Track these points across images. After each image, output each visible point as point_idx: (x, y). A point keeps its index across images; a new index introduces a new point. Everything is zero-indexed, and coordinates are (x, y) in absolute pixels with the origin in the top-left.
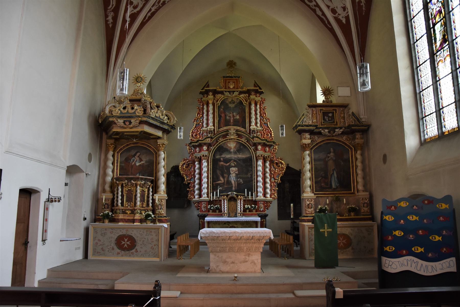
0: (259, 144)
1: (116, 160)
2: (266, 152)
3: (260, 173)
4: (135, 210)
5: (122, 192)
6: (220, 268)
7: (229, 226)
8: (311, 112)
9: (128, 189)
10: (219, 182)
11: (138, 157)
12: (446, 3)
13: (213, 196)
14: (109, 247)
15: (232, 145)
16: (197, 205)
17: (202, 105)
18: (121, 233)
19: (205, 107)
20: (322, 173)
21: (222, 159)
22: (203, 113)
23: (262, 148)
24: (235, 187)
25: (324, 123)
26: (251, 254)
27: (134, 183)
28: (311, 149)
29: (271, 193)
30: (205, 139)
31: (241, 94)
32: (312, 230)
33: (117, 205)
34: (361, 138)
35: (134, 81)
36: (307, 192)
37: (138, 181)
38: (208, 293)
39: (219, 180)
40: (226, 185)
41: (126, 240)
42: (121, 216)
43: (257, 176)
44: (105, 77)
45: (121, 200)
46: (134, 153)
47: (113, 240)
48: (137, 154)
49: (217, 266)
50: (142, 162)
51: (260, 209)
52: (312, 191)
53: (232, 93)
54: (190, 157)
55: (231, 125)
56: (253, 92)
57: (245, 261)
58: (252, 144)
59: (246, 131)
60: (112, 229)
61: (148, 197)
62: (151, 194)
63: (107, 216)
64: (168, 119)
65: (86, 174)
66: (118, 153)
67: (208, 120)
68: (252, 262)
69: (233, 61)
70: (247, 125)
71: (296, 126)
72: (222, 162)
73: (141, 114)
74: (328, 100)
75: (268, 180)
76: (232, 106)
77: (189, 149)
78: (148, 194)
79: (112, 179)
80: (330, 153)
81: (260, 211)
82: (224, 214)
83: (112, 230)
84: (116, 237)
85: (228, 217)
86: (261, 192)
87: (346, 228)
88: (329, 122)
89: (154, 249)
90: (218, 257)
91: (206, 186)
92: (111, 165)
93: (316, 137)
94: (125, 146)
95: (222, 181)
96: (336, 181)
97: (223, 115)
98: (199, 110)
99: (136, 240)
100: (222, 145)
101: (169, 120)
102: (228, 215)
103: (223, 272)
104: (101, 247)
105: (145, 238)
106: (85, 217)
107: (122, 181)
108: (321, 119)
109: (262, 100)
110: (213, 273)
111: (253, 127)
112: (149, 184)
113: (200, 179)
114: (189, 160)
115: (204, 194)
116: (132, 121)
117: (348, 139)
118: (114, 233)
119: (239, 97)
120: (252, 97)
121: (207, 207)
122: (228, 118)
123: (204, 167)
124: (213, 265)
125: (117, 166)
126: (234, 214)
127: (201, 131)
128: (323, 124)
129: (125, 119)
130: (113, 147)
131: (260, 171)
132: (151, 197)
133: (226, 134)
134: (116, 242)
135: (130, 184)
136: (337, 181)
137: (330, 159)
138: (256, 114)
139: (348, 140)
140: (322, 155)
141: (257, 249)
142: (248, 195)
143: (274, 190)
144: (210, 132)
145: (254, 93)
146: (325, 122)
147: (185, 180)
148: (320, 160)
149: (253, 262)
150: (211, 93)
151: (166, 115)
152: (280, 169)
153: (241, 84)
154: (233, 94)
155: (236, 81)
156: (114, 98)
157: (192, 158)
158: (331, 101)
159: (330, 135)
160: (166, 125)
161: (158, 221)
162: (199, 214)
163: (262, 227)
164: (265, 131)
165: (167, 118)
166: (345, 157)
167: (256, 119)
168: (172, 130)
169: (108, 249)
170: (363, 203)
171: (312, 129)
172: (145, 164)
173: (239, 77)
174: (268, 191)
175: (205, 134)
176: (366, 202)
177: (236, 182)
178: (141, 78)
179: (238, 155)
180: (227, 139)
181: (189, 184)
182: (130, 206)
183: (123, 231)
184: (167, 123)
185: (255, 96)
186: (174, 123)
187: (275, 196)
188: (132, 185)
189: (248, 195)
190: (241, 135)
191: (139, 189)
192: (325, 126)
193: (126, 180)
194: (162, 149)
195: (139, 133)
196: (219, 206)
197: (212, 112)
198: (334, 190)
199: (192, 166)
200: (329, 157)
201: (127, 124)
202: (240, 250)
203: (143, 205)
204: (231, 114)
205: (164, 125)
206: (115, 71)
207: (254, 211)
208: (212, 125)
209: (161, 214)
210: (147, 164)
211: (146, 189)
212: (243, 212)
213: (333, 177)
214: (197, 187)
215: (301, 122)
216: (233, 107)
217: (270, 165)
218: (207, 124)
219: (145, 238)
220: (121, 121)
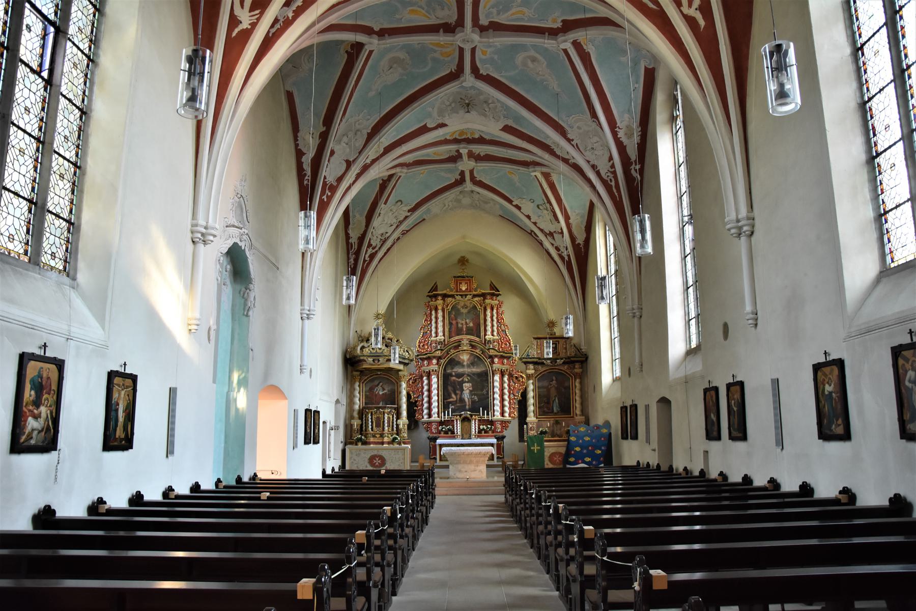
0: (496, 356)
2: (503, 364)
3: (497, 390)
4: (383, 434)
5: (372, 419)
8: (535, 343)
10: (451, 400)
12: (893, 13)
13: (445, 415)
17: (430, 309)
18: (373, 454)
19: (433, 312)
21: (454, 373)
24: (469, 405)
28: (535, 378)
29: (510, 411)
30: (435, 351)
33: (369, 431)
34: (580, 368)
38: (450, 487)
39: (450, 397)
41: (377, 459)
42: (372, 440)
43: (494, 393)
44: (348, 313)
47: (367, 460)
49: (455, 474)
52: (535, 415)
53: (464, 297)
54: (418, 371)
55: (463, 334)
57: (475, 470)
58: (487, 356)
60: (365, 450)
61: (393, 423)
62: (395, 420)
63: (360, 440)
66: (363, 383)
67: (436, 328)
70: (482, 334)
75: (506, 397)
78: (393, 420)
80: (553, 380)
81: (497, 432)
84: (368, 457)
85: (462, 439)
86: (498, 411)
91: (437, 404)
92: (358, 395)
93: (540, 367)
97: (454, 322)
98: (427, 316)
103: (459, 478)
111: (489, 337)
112: (394, 411)
113: (430, 397)
115: (434, 414)
120: (487, 301)
121: (438, 428)
122: (460, 325)
123: (434, 383)
126: (468, 435)
131: (497, 387)
132: (395, 423)
133: (458, 345)
138: (492, 320)
140: (545, 383)
142: (483, 414)
143: (514, 408)
149: (480, 471)
150: (440, 298)
153: (475, 286)
154: (466, 297)
156: (356, 331)
164: (503, 340)
166: (566, 384)
167: (493, 326)
172: (388, 393)
173: (472, 277)
174: (506, 409)
175: (434, 345)
181: (416, 402)
189: (483, 414)
196: (451, 427)
197: (442, 319)
198: (556, 414)
200: (551, 385)
202: (471, 462)
204: (463, 320)
207: (490, 432)
208: (442, 334)
210: (389, 392)
212: (478, 433)
213: (555, 403)
214: (426, 405)
217: (509, 380)
220: (371, 360)
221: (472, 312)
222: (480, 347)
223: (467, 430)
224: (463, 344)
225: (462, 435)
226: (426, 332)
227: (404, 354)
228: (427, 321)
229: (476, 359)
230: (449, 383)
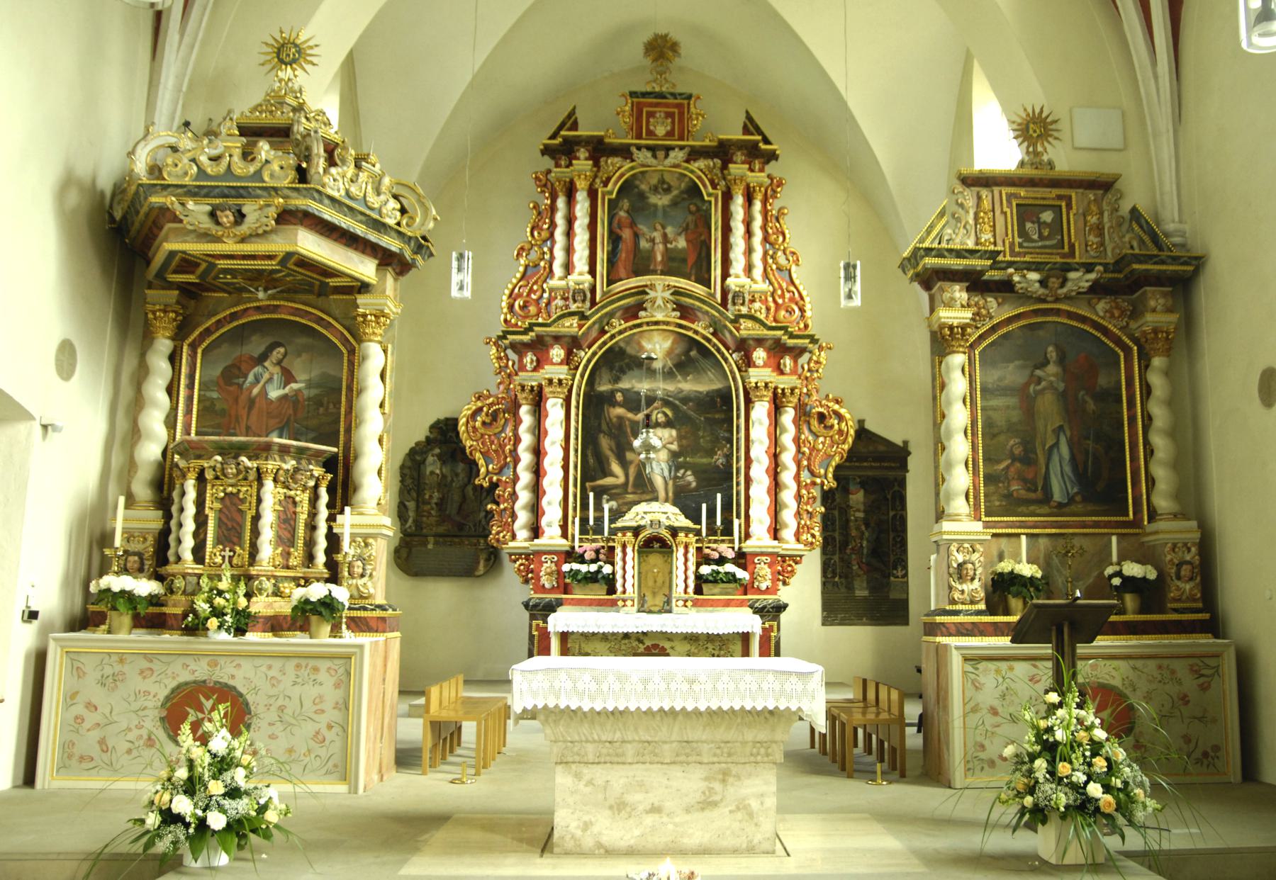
0: (760, 342)
1: (183, 377)
5: (200, 503)
6: (600, 834)
7: (641, 645)
8: (970, 203)
9: (224, 491)
10: (608, 481)
11: (279, 363)
14: (131, 736)
15: (658, 347)
16: (521, 565)
17: (551, 194)
18: (185, 677)
19: (561, 203)
20: (1012, 442)
21: (619, 397)
22: (553, 225)
23: (769, 357)
25: (1020, 245)
26: (734, 773)
27: (249, 468)
28: (972, 347)
31: (695, 160)
32: (977, 669)
33: (179, 559)
35: (269, 58)
36: (954, 518)
37: (267, 459)
40: (633, 493)
45: (196, 535)
46: (262, 349)
48: (275, 353)
49: (586, 826)
50: (294, 386)
51: (759, 582)
53: (661, 154)
54: (502, 387)
55: (654, 272)
56: (739, 153)
59: (710, 294)
61: (312, 527)
62: (323, 513)
64: (403, 211)
65: (45, 427)
66: (193, 347)
67: (569, 250)
68: (738, 809)
69: (666, 35)
70: (716, 272)
71: (917, 255)
72: (621, 405)
73: (285, 183)
74: (1037, 160)
75: (787, 477)
76: (660, 203)
77: (499, 358)
78: (313, 514)
79: (164, 453)
80: (1045, 363)
81: (759, 591)
82: (624, 601)
83: (151, 661)
87: (1116, 663)
88: (1040, 244)
89: (327, 742)
90: (590, 783)
94: (225, 318)
95: (617, 477)
96: (1069, 477)
97: (626, 234)
98: (539, 213)
99: (251, 703)
100: (622, 345)
101: (406, 215)
102: (639, 603)
104: (95, 735)
105: (290, 697)
106: (34, 608)
107: (199, 457)
108: (1010, 232)
109: (772, 184)
110: (567, 853)
112: (318, 471)
114: (498, 398)
116: (245, 210)
117: (1117, 313)
118: (155, 674)
119: (686, 169)
122: (644, 244)
124: (566, 822)
125: (190, 399)
126: (660, 600)
127: (544, 291)
128: (1017, 249)
129: (217, 201)
130: (175, 320)
134: (164, 714)
135: (231, 470)
136: (1070, 474)
137: (1044, 389)
138: (749, 233)
139: (1117, 315)
141: (762, 751)
143: (811, 515)
144: (578, 294)
145: (743, 154)
146: (1025, 244)
147: (479, 471)
148: (1004, 391)
150: (582, 153)
151: (396, 197)
152: (831, 437)
154: (667, 156)
155: (676, 111)
157: (508, 389)
158: (1051, 164)
159: (1047, 296)
160: (393, 234)
161: (346, 623)
162: (530, 599)
163: (764, 652)
164: (782, 296)
165: (398, 206)
166: (1103, 381)
167: (749, 251)
168: (419, 258)
169: (130, 745)
170: (1176, 562)
171: (979, 268)
172: (306, 393)
175: (559, 302)
176: (1188, 558)
177: (671, 483)
178: (296, 46)
179: (679, 382)
180: (638, 321)
181: (494, 486)
182: (230, 562)
183: (195, 668)
184: (396, 227)
185: (747, 166)
186: (423, 231)
187: (813, 536)
188: (241, 477)
190: (692, 309)
191: (271, 495)
192: (1027, 259)
193: (220, 454)
194: (374, 333)
195: (277, 265)
199: (506, 420)
200: (1039, 380)
201: (225, 220)
203: (287, 560)
204: (655, 229)
205: (385, 234)
206: (190, 13)
208: (586, 268)
209: (361, 597)
210: (314, 392)
211: (303, 491)
213: (1056, 458)
215: (935, 239)
216: (664, 207)
217: (796, 422)
218: (568, 267)
219: (290, 697)
220: (197, 210)
221: (686, 203)
222: (707, 313)
223: (660, 580)
224: (653, 301)
225: (642, 599)
226: (537, 266)
227: (374, 200)
228: (542, 229)
229: (693, 353)
230: (604, 427)
